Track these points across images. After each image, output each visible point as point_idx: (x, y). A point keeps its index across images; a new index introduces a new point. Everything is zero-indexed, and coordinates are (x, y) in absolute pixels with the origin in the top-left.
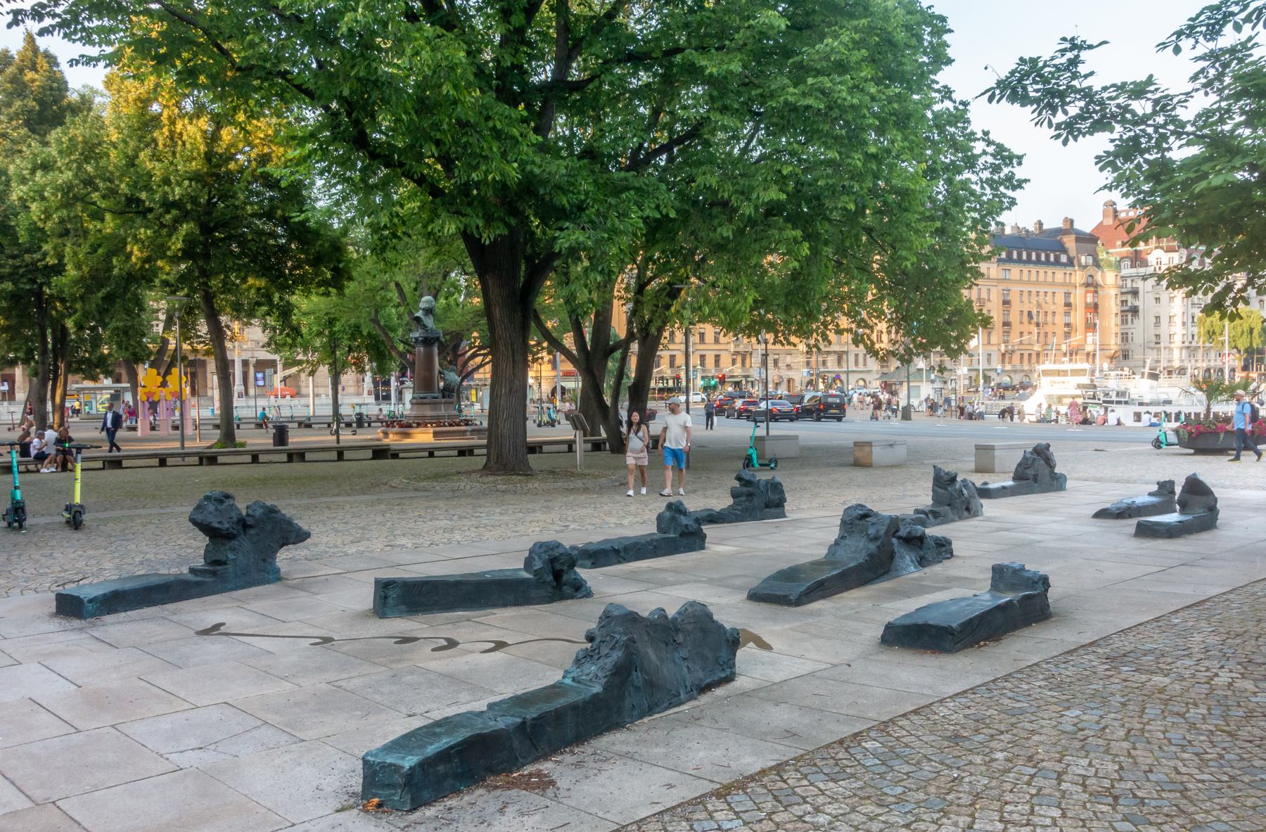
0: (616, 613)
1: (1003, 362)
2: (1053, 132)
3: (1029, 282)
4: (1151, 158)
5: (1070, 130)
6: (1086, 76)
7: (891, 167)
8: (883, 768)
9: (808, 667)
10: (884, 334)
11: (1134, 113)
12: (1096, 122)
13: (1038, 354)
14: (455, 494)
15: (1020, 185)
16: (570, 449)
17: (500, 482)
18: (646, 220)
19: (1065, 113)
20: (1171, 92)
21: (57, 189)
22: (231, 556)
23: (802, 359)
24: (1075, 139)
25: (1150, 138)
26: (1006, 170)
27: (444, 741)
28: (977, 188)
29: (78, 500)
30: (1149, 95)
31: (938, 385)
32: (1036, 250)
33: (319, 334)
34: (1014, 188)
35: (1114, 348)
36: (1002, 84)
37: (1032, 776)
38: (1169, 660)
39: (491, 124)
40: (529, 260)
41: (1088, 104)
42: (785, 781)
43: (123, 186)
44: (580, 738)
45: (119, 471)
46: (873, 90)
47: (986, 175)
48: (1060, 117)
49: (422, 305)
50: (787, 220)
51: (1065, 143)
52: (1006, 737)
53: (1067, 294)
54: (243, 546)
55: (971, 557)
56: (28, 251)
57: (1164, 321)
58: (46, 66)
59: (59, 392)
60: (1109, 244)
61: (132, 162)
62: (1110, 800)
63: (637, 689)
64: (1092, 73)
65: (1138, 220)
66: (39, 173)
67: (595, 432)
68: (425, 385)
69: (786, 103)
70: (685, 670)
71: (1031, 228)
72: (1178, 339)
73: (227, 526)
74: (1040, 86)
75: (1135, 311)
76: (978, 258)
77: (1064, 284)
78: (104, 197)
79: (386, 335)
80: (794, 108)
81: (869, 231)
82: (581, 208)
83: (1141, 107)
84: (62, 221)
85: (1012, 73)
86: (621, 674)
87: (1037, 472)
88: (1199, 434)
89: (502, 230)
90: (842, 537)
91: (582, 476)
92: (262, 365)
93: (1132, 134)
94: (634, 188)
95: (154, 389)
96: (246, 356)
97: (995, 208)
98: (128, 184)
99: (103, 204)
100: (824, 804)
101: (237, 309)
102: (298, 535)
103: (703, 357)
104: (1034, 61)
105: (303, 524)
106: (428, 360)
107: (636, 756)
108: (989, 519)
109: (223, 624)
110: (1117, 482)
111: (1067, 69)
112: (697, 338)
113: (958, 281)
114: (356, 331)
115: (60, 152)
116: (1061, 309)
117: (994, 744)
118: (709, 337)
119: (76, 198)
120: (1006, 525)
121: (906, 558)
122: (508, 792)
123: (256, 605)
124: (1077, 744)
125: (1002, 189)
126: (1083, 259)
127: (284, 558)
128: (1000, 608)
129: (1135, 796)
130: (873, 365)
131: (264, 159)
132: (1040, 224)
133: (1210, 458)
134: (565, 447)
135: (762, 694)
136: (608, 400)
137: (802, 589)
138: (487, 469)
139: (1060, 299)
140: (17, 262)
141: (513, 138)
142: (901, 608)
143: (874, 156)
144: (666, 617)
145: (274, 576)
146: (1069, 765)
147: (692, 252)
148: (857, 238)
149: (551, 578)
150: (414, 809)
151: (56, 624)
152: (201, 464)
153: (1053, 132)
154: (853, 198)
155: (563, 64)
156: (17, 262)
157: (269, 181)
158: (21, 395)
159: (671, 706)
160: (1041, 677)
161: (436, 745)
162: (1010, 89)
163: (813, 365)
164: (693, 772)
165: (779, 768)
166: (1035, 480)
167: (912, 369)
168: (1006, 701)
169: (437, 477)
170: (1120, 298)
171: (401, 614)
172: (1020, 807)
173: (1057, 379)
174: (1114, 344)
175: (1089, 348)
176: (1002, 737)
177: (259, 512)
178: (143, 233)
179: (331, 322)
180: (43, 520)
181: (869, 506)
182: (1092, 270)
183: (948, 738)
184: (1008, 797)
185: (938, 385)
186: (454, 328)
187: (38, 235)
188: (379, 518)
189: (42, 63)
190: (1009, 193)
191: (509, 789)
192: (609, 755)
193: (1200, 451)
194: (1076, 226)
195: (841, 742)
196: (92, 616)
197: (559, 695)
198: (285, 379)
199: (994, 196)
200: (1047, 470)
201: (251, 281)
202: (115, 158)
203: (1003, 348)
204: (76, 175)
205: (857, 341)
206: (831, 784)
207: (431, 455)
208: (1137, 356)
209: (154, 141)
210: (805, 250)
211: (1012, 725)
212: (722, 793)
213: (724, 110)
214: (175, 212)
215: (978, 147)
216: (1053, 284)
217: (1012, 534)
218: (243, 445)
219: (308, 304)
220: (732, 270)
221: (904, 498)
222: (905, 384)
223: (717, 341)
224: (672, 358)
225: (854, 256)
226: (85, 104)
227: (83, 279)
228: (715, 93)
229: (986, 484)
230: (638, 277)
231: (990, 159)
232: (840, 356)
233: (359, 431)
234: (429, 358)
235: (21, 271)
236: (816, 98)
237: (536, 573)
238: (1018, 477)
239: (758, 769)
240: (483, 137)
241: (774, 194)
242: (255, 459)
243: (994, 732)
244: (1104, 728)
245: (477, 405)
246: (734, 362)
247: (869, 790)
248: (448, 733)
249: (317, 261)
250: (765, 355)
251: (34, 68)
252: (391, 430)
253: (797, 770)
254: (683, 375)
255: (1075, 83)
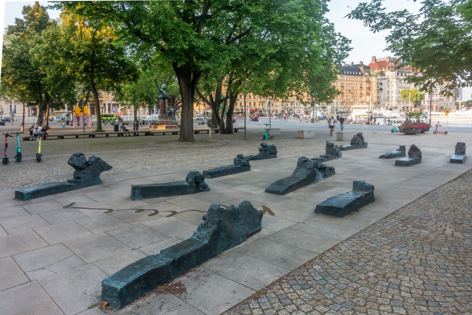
0: (215, 209)
1: (341, 105)
2: (371, 29)
3: (349, 81)
4: (405, 38)
5: (377, 28)
6: (383, 9)
7: (311, 43)
8: (324, 282)
9: (287, 224)
10: (306, 97)
11: (399, 22)
12: (386, 25)
13: (352, 102)
14: (169, 149)
15: (350, 49)
16: (208, 132)
17: (184, 144)
18: (232, 60)
19: (375, 22)
20: (413, 14)
21: (43, 49)
22: (82, 176)
23: (281, 104)
24: (378, 31)
25: (405, 30)
26: (346, 45)
27: (138, 273)
28: (336, 51)
29: (39, 152)
30: (405, 16)
31: (322, 112)
32: (349, 71)
33: (131, 96)
34: (348, 50)
35: (375, 101)
36: (353, 12)
37: (388, 287)
38: (425, 222)
39: (180, 29)
40: (194, 73)
41: (383, 20)
42: (283, 290)
43: (65, 49)
44: (199, 263)
45: (62, 140)
46: (305, 18)
47: (339, 47)
48: (373, 24)
49: (162, 87)
50: (277, 60)
51: (374, 32)
52: (372, 263)
53: (361, 84)
54: (88, 173)
55: (341, 174)
56: (36, 69)
57: (390, 92)
58: (42, 11)
59: (47, 114)
60: (374, 69)
61: (68, 41)
62: (424, 303)
63: (223, 239)
64: (385, 8)
65: (399, 59)
66: (37, 44)
67: (216, 127)
68: (163, 112)
69: (277, 22)
70: (242, 229)
71: (350, 64)
72: (394, 98)
73: (81, 165)
74: (367, 13)
75: (381, 89)
76: (336, 73)
77: (360, 81)
78: (59, 52)
79: (152, 96)
80: (280, 24)
81: (303, 64)
82: (210, 56)
83: (401, 20)
84: (45, 60)
85: (357, 8)
86: (216, 235)
87: (358, 142)
88: (407, 128)
89: (184, 63)
90: (298, 168)
91: (211, 142)
92: (114, 105)
93: (398, 29)
94: (228, 50)
95: (78, 113)
96: (109, 102)
97: (341, 58)
98: (66, 48)
99: (59, 54)
100: (301, 305)
101: (103, 88)
102: (108, 168)
103: (250, 103)
104: (365, 4)
105: (110, 163)
106: (166, 104)
107: (221, 273)
108: (344, 159)
109: (74, 203)
110: (383, 144)
111: (376, 7)
112: (248, 97)
113: (329, 80)
114: (142, 95)
115: (45, 38)
116: (359, 89)
117: (367, 267)
118: (252, 97)
119: (49, 52)
120: (350, 161)
121: (320, 175)
122: (165, 295)
123: (90, 195)
124: (402, 268)
125: (344, 51)
126: (366, 74)
127: (103, 175)
128: (358, 199)
129: (435, 301)
130: (302, 106)
131: (110, 41)
132: (353, 63)
133: (411, 136)
134: (206, 132)
135: (271, 238)
136: (220, 115)
137: (285, 189)
138: (180, 140)
139: (359, 86)
140: (32, 73)
141: (188, 33)
142: (322, 197)
143: (305, 39)
144: (234, 209)
145: (99, 182)
146: (401, 280)
147: (247, 71)
148: (299, 66)
149: (195, 185)
150: (122, 307)
151: (16, 202)
152: (90, 137)
153: (371, 29)
154: (298, 53)
155: (205, 10)
156: (32, 73)
157: (112, 48)
158: (38, 114)
159: (237, 244)
160: (378, 230)
161: (134, 276)
162: (357, 14)
163: (284, 105)
164: (244, 283)
165: (280, 281)
166: (358, 145)
167: (315, 107)
168: (368, 243)
169: (163, 143)
170: (377, 85)
171: (140, 199)
172: (387, 308)
173: (358, 110)
174: (375, 99)
175: (368, 101)
176: (370, 263)
177: (93, 160)
178: (71, 64)
179: (134, 93)
180: (29, 158)
181: (307, 157)
182: (368, 77)
183: (347, 264)
184: (380, 301)
185: (322, 112)
186: (173, 94)
187: (37, 63)
188: (142, 158)
189: (41, 10)
190: (347, 52)
191: (166, 293)
192: (210, 272)
193: (407, 134)
194: (364, 64)
195: (305, 265)
196: (27, 199)
197: (190, 245)
198: (121, 109)
199: (342, 53)
200: (361, 141)
201: (106, 79)
202: (62, 40)
203: (341, 100)
204: (49, 45)
205: (298, 98)
206: (303, 291)
207: (164, 134)
208: (382, 103)
209: (75, 34)
210: (281, 70)
211: (373, 256)
212: (256, 297)
213: (257, 24)
214: (81, 57)
215: (337, 38)
216: (357, 81)
217: (353, 165)
218: (104, 131)
219: (126, 86)
220: (259, 76)
221: (316, 151)
222: (312, 112)
223: (254, 98)
224: (241, 103)
225: (297, 72)
226: (55, 23)
227: (53, 78)
228: (254, 19)
229: (342, 146)
230: (230, 78)
231: (341, 42)
232: (292, 103)
233: (143, 126)
234: (164, 103)
235: (33, 76)
236: (287, 20)
237: (190, 183)
238: (352, 143)
239: (272, 282)
240: (177, 33)
241: (273, 51)
242: (107, 136)
243: (366, 260)
244: (410, 259)
245: (178, 118)
246: (260, 105)
247: (319, 295)
248: (141, 268)
249: (128, 73)
250: (269, 103)
251: (38, 11)
252: (152, 126)
253: (288, 282)
254: (244, 109)
255: (379, 12)
